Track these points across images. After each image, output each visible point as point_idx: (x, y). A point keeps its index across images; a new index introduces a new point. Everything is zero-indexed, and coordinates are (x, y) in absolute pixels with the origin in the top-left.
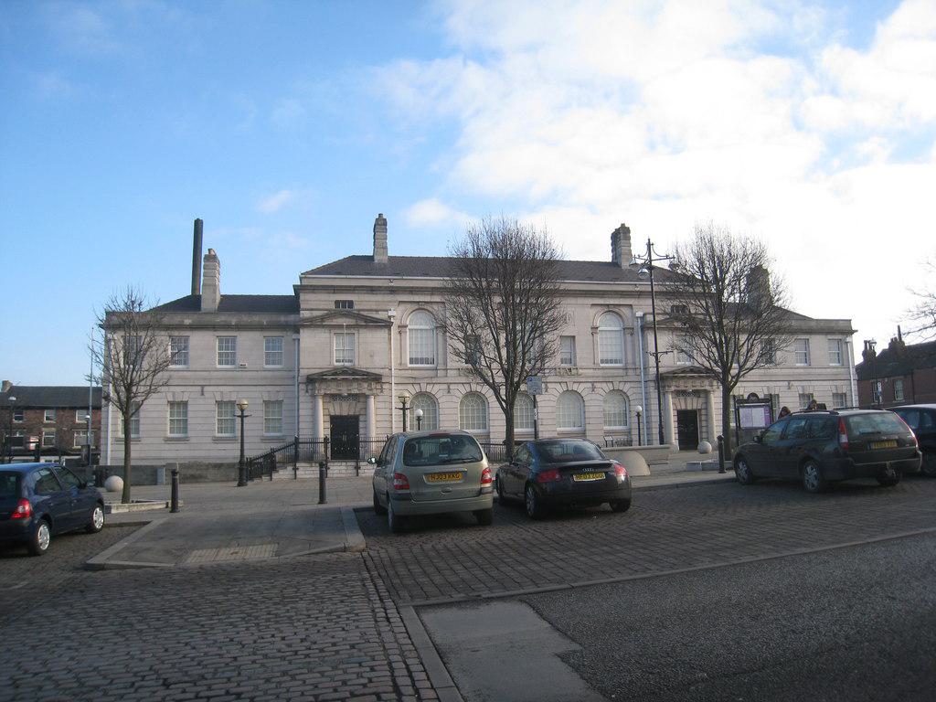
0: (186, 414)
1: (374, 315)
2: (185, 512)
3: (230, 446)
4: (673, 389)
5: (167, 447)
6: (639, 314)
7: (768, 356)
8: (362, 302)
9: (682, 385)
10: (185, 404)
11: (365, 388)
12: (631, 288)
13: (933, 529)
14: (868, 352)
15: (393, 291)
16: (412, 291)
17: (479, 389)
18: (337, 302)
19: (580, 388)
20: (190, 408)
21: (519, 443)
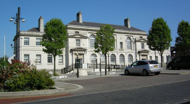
0: (41, 57)
1: (84, 35)
2: (108, 75)
3: (51, 66)
4: (141, 54)
5: (59, 66)
6: (134, 38)
7: (37, 44)
8: (81, 32)
9: (143, 54)
10: (28, 55)
11: (83, 52)
12: (86, 28)
13: (189, 80)
14: (168, 48)
15: (87, 30)
16: (91, 30)
17: (95, 53)
18: (75, 32)
19: (124, 54)
20: (30, 56)
21: (57, 70)
